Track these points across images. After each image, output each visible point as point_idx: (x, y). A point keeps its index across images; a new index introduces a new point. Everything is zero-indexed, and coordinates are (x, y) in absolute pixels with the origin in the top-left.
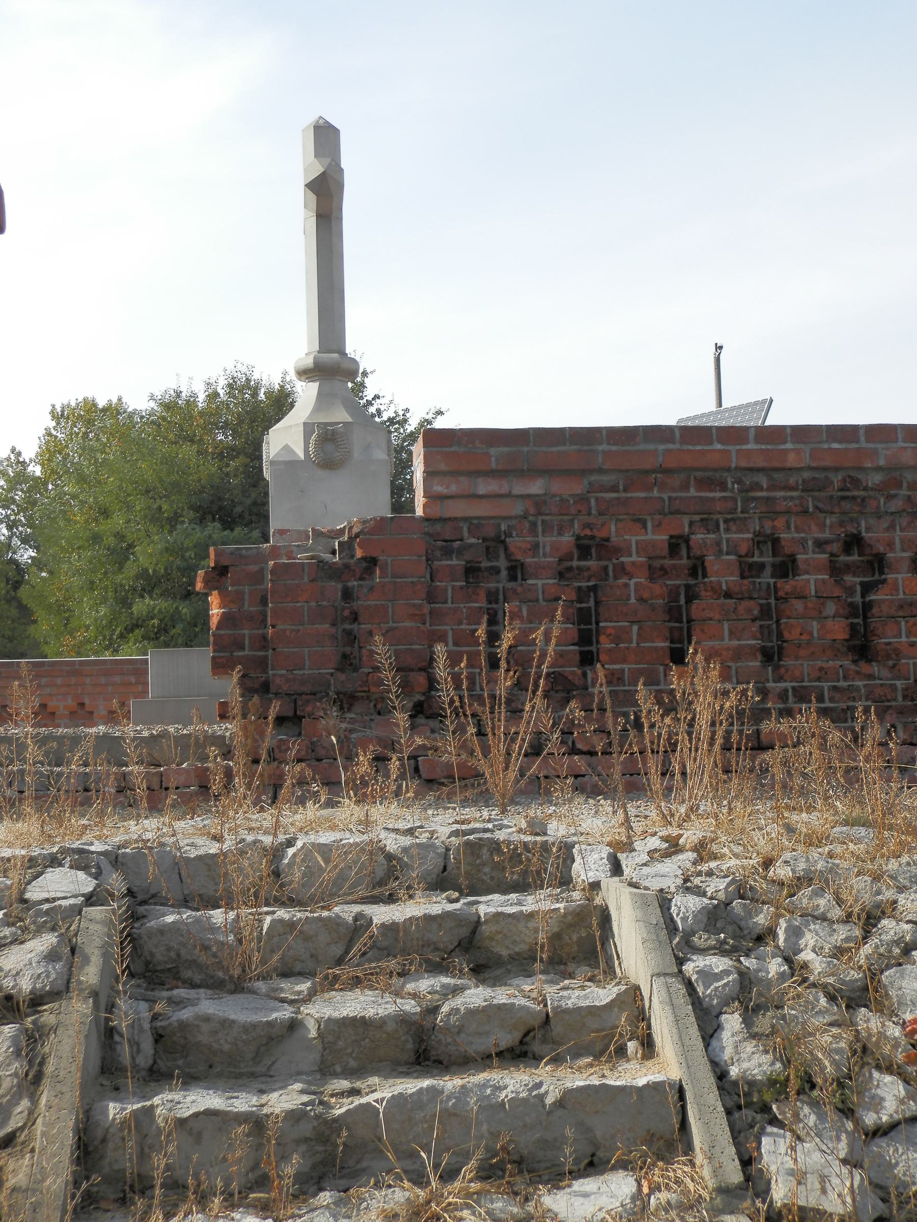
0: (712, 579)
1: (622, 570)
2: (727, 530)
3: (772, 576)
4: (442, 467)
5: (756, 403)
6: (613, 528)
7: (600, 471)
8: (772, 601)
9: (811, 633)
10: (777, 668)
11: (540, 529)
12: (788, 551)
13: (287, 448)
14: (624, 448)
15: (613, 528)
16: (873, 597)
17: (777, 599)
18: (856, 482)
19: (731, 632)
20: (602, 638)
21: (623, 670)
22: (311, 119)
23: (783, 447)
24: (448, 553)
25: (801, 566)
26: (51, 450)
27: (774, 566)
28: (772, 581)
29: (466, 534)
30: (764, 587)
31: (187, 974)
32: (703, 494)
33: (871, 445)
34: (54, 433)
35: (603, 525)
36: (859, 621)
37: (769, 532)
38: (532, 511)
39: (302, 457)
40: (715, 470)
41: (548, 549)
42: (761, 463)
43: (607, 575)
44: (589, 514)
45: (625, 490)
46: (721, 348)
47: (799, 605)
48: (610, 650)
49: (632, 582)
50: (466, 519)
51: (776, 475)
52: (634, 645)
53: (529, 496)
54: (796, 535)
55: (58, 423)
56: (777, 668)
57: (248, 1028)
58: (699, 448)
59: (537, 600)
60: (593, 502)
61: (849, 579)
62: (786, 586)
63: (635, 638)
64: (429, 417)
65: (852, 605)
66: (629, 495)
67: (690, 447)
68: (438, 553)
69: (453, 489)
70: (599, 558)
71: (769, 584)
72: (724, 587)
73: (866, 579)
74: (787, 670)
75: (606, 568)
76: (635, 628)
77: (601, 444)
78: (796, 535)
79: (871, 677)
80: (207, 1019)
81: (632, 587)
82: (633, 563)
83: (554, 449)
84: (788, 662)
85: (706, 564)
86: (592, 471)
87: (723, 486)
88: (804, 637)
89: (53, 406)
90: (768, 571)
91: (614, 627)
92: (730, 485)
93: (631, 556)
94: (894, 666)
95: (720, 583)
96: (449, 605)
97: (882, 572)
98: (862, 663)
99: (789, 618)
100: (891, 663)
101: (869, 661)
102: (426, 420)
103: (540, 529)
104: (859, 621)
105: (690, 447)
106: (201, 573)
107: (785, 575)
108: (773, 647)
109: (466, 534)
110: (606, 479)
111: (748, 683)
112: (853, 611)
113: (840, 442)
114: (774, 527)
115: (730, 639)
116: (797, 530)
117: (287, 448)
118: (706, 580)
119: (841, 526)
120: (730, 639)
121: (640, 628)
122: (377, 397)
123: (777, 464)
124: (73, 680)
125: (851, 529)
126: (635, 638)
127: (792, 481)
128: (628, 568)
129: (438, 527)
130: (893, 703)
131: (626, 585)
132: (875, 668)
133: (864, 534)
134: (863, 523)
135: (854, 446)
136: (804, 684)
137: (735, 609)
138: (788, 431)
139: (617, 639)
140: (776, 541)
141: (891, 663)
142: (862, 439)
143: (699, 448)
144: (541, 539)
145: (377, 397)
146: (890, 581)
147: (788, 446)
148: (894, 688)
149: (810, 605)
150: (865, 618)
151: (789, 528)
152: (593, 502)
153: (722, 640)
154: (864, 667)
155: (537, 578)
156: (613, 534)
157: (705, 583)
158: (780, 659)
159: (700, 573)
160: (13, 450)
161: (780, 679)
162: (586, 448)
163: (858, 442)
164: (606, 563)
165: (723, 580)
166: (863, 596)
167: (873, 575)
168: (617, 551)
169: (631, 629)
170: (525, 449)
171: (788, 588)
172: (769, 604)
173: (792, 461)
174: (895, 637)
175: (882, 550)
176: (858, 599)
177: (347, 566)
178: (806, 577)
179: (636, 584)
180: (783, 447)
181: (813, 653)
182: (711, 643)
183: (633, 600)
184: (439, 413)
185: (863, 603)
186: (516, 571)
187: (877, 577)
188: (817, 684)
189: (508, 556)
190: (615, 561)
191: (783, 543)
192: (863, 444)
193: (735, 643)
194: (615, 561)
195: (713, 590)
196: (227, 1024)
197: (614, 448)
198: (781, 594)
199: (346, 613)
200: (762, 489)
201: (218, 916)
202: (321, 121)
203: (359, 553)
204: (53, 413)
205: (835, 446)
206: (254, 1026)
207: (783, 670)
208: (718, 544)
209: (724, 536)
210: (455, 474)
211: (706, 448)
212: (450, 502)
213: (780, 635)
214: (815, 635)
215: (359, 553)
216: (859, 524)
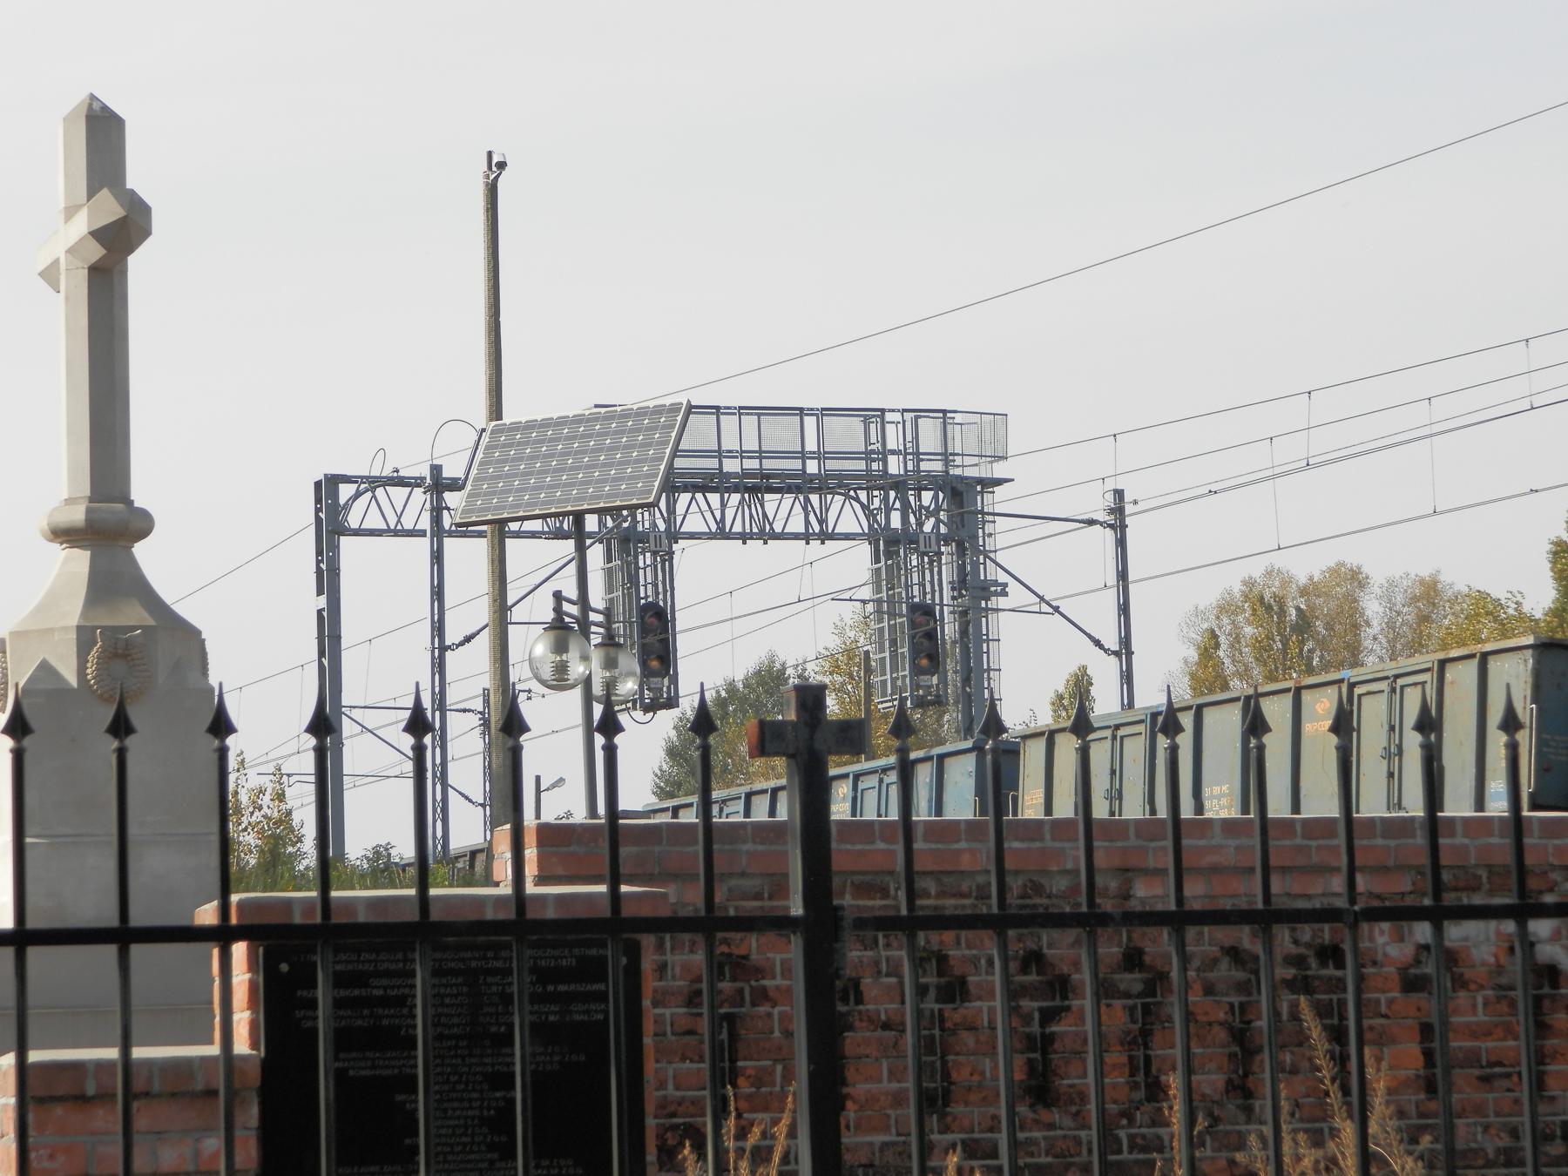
0: (870, 1007)
1: (762, 996)
2: (888, 946)
3: (937, 1001)
5: (659, 410)
6: (754, 944)
7: (743, 874)
8: (937, 1032)
9: (983, 1074)
10: (943, 1116)
12: (957, 972)
13: (45, 667)
14: (773, 847)
15: (754, 944)
16: (1055, 1028)
17: (942, 1029)
18: (1038, 889)
19: (891, 1072)
22: (77, 98)
23: (956, 846)
25: (973, 990)
27: (938, 987)
28: (936, 1007)
30: (927, 1014)
32: (860, 902)
33: (1057, 844)
36: (1037, 1056)
37: (936, 948)
39: (73, 681)
40: (877, 873)
41: (678, 970)
43: (743, 999)
45: (771, 898)
46: (502, 165)
47: (969, 1039)
48: (750, 1095)
49: (776, 1010)
51: (946, 880)
52: (778, 1088)
54: (967, 952)
56: (943, 1116)
58: (859, 847)
59: (664, 1034)
61: (1027, 1004)
62: (954, 1014)
63: (778, 1080)
65: (1030, 1037)
66: (775, 903)
67: (849, 847)
70: (734, 979)
71: (932, 1011)
72: (883, 1017)
73: (1045, 1004)
74: (955, 1118)
75: (741, 991)
76: (779, 1068)
77: (744, 842)
78: (967, 952)
79: (1051, 1126)
81: (776, 1017)
82: (778, 988)
84: (957, 1109)
85: (862, 988)
87: (885, 893)
88: (976, 1078)
90: (932, 994)
91: (754, 1068)
92: (892, 892)
93: (774, 978)
94: (1077, 1113)
95: (878, 1012)
97: (1064, 997)
98: (1039, 1107)
99: (958, 1054)
100: (1074, 1109)
101: (1048, 1105)
104: (1037, 1056)
105: (849, 847)
107: (952, 1000)
108: (936, 1089)
110: (747, 884)
111: (888, 1116)
112: (1030, 1043)
113: (1022, 840)
114: (941, 942)
115: (890, 1081)
116: (969, 947)
117: (45, 667)
118: (861, 1007)
119: (1019, 941)
120: (890, 1081)
121: (784, 1068)
123: (949, 868)
125: (1031, 945)
126: (778, 1080)
127: (965, 887)
128: (771, 994)
130: (1076, 1159)
131: (769, 1015)
132: (1055, 1116)
133: (1045, 951)
134: (1045, 938)
135: (1038, 844)
136: (976, 1135)
137: (896, 1043)
138: (963, 826)
139: (758, 1082)
140: (942, 959)
141: (1074, 1109)
142: (1048, 836)
143: (859, 847)
144: (669, 957)
146: (1074, 1009)
147: (963, 845)
148: (1078, 1141)
149: (983, 1038)
150: (1045, 1053)
151: (959, 943)
153: (880, 1081)
154: (1045, 1115)
155: (665, 1007)
156: (754, 950)
157: (860, 1012)
158: (946, 1105)
159: (852, 998)
161: (945, 1129)
162: (727, 847)
163: (1042, 839)
164: (739, 984)
165: (882, 1008)
166: (1043, 1024)
167: (1053, 999)
168: (759, 972)
169: (774, 1071)
170: (657, 849)
171: (957, 1017)
172: (932, 1037)
173: (966, 863)
174: (1079, 1077)
175: (1065, 970)
176: (1035, 1028)
178: (978, 1003)
179: (780, 1013)
180: (956, 846)
181: (985, 1098)
182: (868, 1086)
183: (777, 1034)
185: (1043, 1035)
187: (1058, 1002)
188: (989, 1135)
190: (753, 983)
191: (952, 962)
192: (1049, 843)
193: (895, 1085)
194: (753, 983)
195: (870, 1020)
197: (760, 848)
198: (948, 1024)
200: (929, 897)
202: (96, 106)
207: (949, 1119)
208: (877, 963)
209: (883, 953)
211: (868, 847)
213: (946, 1075)
214: (988, 1075)
216: (1040, 939)
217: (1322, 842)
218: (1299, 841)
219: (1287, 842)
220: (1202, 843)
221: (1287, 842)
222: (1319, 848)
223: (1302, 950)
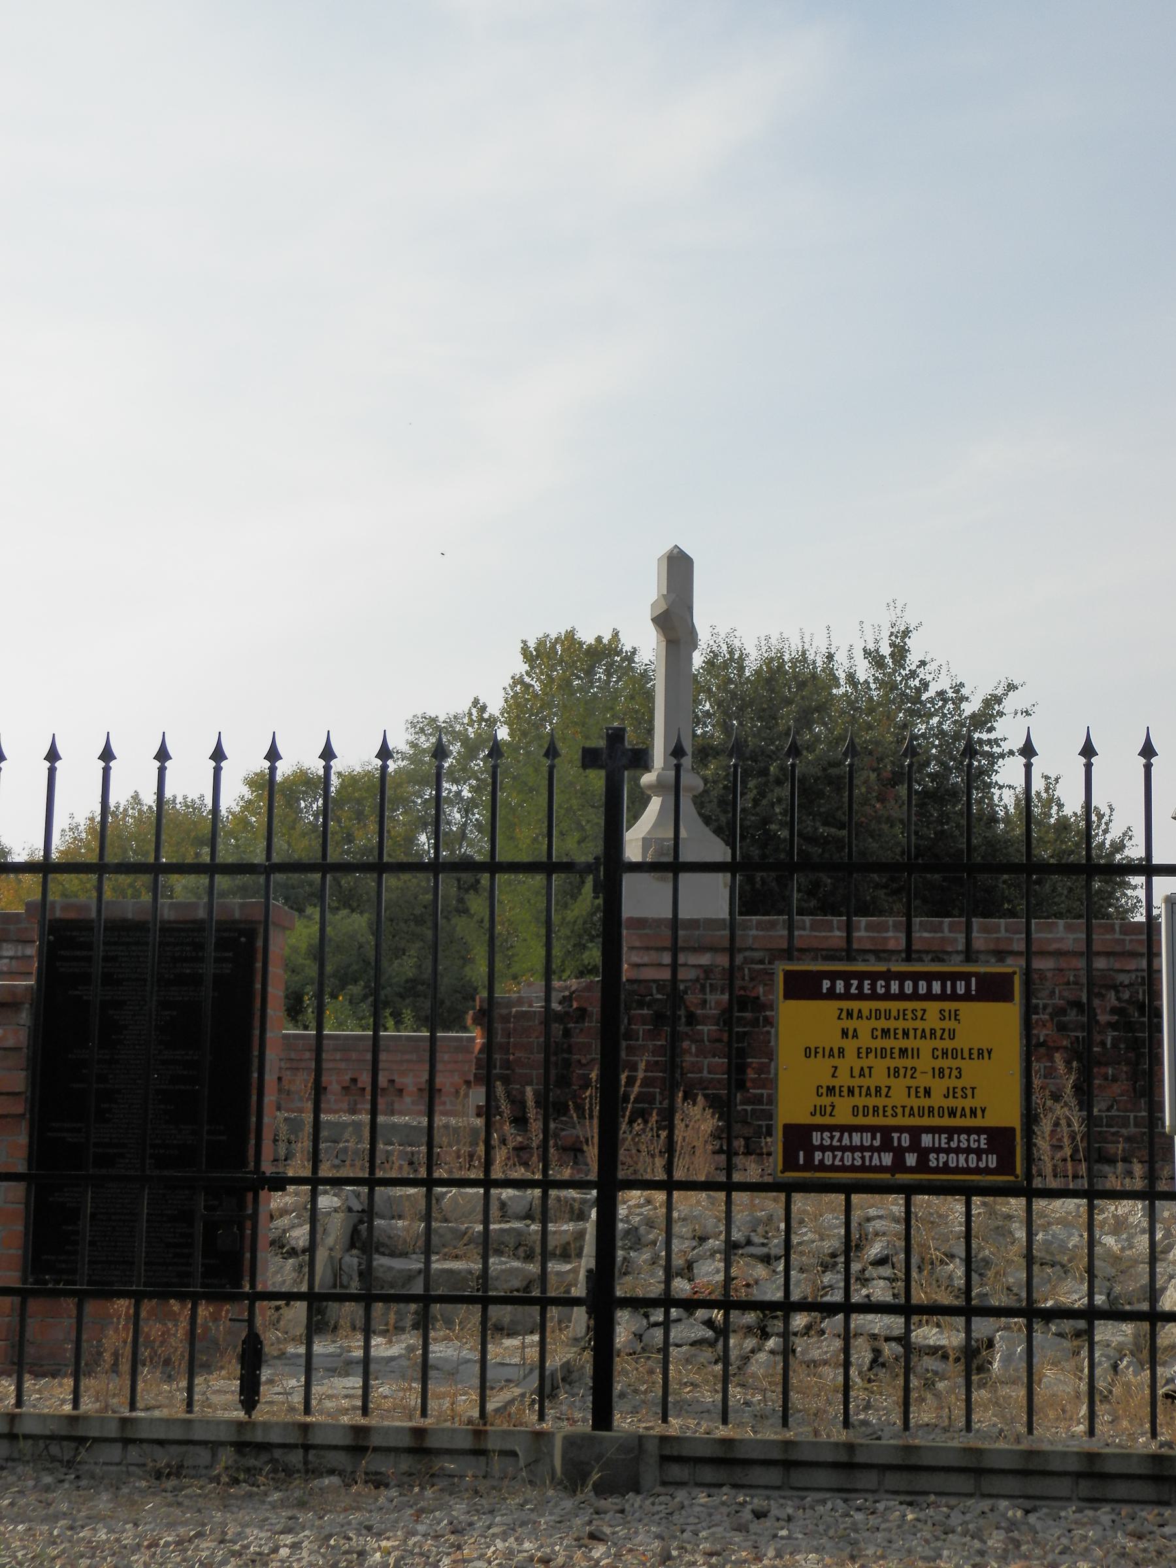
4: (637, 944)
7: (752, 949)
11: (708, 990)
15: (761, 990)
20: (749, 1071)
21: (762, 1095)
22: (666, 548)
23: (885, 935)
24: (641, 1004)
26: (520, 703)
29: (654, 991)
31: (382, 1250)
33: (952, 935)
34: (527, 679)
35: (753, 988)
38: (702, 976)
40: (837, 950)
41: (713, 1004)
42: (868, 946)
44: (743, 979)
50: (654, 981)
53: (700, 966)
55: (532, 667)
57: (400, 1271)
60: (746, 971)
64: (999, 692)
68: (634, 1005)
69: (646, 960)
80: (382, 1266)
83: (718, 933)
86: (746, 949)
89: (524, 642)
96: (640, 1042)
102: (995, 696)
103: (708, 990)
106: (471, 1012)
109: (654, 991)
110: (757, 955)
122: (923, 663)
123: (881, 948)
124: (460, 1057)
129: (635, 986)
135: (939, 935)
142: (946, 929)
144: (708, 997)
145: (923, 663)
147: (890, 934)
152: (746, 971)
160: (476, 702)
177: (567, 1013)
180: (885, 935)
184: (1011, 687)
186: (692, 1019)
189: (686, 1007)
196: (390, 1269)
197: (761, 933)
199: (565, 1046)
201: (400, 1223)
202: (675, 551)
203: (575, 1005)
204: (525, 650)
205: (926, 935)
206: (403, 1270)
210: (648, 949)
212: (642, 969)
215: (575, 1005)
217: (1134, 937)
218: (1117, 936)
219: (1108, 937)
220: (1050, 936)
221: (1108, 937)
222: (1131, 941)
223: (1123, 1005)
